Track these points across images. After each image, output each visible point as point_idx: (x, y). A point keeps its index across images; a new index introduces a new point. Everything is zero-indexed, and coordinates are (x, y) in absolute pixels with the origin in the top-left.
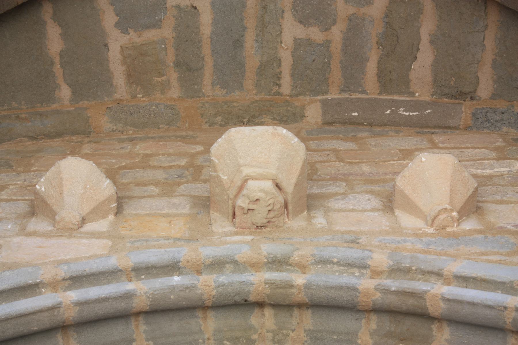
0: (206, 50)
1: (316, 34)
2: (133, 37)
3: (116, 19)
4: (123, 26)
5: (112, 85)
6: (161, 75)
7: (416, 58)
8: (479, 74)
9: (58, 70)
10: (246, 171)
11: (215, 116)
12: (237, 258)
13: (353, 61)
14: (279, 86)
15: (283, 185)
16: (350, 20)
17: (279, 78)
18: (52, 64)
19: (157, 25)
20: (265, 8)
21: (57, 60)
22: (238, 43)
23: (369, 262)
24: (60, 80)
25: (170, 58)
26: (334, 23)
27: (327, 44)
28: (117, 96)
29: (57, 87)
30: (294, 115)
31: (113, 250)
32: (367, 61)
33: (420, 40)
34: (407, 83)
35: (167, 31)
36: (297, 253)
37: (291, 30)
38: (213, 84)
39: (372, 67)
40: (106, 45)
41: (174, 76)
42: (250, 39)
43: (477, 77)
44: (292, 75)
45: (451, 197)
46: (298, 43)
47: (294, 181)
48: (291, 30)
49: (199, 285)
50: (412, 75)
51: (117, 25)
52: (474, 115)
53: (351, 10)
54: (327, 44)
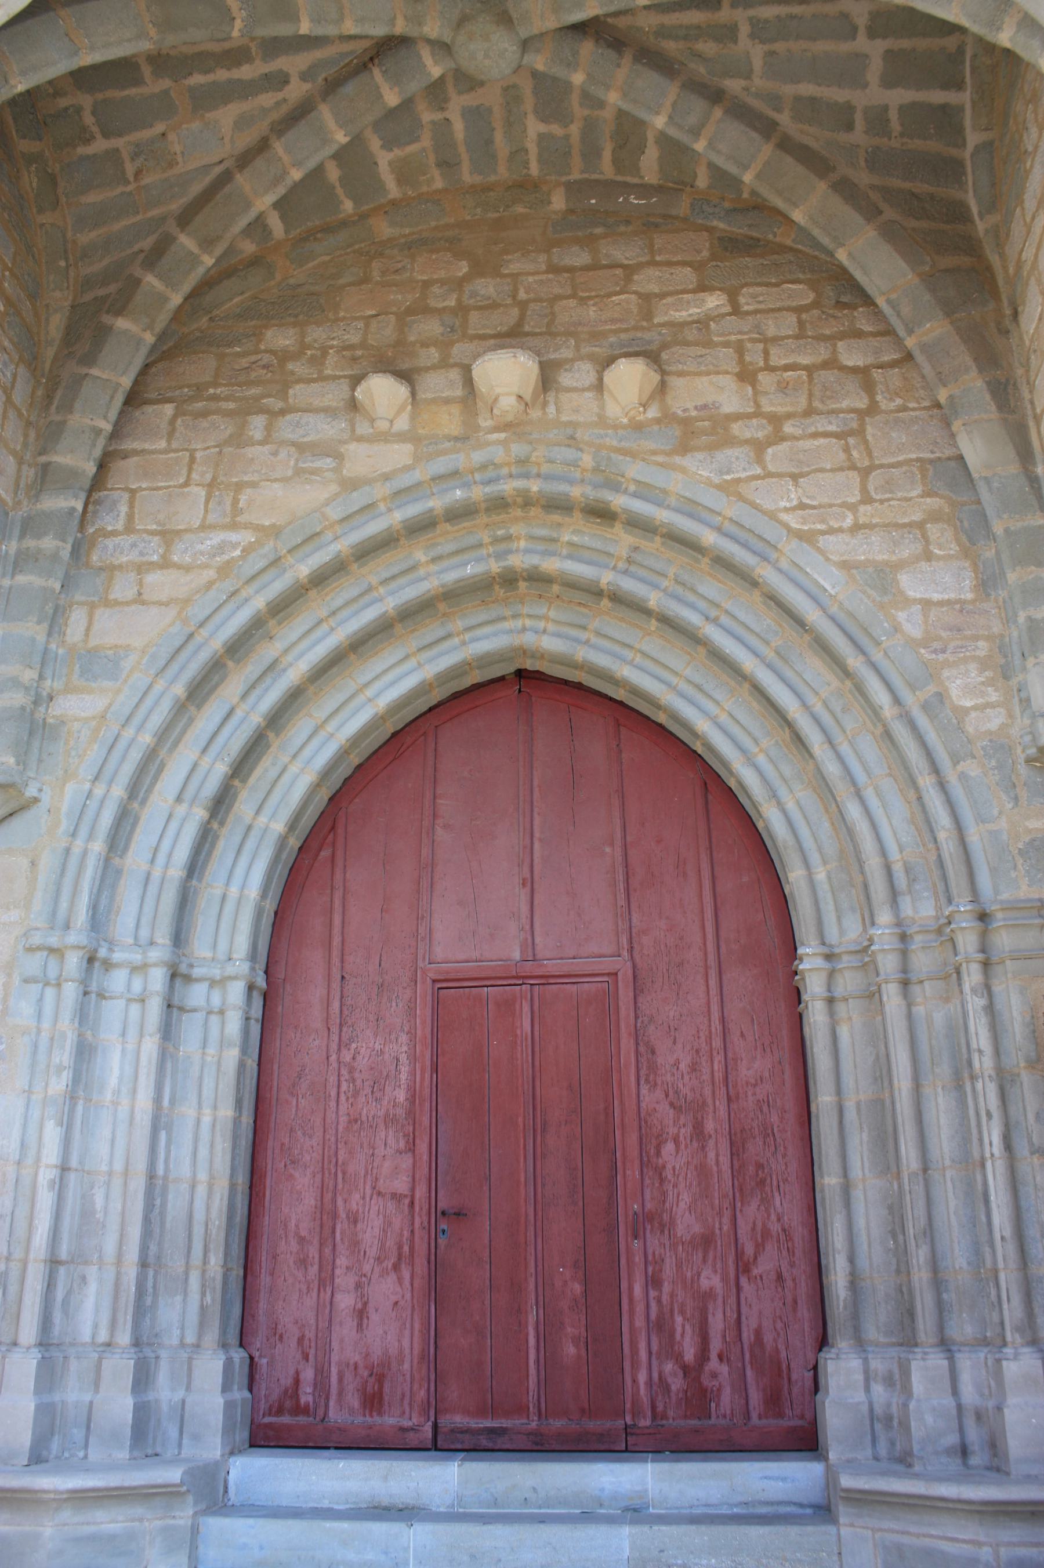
0: (462, 149)
1: (556, 129)
2: (398, 152)
3: (380, 143)
4: (387, 146)
5: (385, 190)
6: (425, 174)
7: (644, 152)
8: (698, 171)
9: (339, 191)
10: (498, 390)
11: (475, 207)
12: (496, 461)
13: (591, 153)
14: (528, 169)
15: (524, 396)
16: (586, 120)
17: (528, 163)
18: (334, 188)
19: (417, 139)
20: (510, 111)
21: (337, 184)
22: (489, 142)
23: (580, 463)
24: (342, 197)
25: (432, 159)
26: (572, 122)
27: (567, 137)
28: (391, 196)
29: (342, 202)
30: (542, 201)
31: (417, 458)
32: (603, 149)
33: (646, 140)
34: (638, 169)
35: (426, 141)
36: (535, 454)
37: (534, 127)
38: (471, 173)
39: (607, 155)
40: (376, 163)
41: (436, 173)
42: (499, 137)
43: (695, 173)
44: (539, 161)
45: (640, 395)
46: (541, 137)
47: (530, 390)
48: (534, 127)
49: (473, 496)
50: (641, 164)
51: (382, 147)
52: (692, 205)
53: (586, 112)
54: (567, 137)
